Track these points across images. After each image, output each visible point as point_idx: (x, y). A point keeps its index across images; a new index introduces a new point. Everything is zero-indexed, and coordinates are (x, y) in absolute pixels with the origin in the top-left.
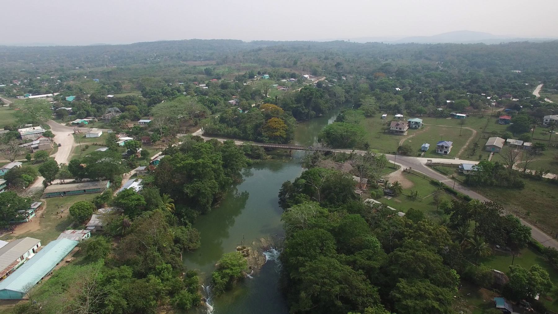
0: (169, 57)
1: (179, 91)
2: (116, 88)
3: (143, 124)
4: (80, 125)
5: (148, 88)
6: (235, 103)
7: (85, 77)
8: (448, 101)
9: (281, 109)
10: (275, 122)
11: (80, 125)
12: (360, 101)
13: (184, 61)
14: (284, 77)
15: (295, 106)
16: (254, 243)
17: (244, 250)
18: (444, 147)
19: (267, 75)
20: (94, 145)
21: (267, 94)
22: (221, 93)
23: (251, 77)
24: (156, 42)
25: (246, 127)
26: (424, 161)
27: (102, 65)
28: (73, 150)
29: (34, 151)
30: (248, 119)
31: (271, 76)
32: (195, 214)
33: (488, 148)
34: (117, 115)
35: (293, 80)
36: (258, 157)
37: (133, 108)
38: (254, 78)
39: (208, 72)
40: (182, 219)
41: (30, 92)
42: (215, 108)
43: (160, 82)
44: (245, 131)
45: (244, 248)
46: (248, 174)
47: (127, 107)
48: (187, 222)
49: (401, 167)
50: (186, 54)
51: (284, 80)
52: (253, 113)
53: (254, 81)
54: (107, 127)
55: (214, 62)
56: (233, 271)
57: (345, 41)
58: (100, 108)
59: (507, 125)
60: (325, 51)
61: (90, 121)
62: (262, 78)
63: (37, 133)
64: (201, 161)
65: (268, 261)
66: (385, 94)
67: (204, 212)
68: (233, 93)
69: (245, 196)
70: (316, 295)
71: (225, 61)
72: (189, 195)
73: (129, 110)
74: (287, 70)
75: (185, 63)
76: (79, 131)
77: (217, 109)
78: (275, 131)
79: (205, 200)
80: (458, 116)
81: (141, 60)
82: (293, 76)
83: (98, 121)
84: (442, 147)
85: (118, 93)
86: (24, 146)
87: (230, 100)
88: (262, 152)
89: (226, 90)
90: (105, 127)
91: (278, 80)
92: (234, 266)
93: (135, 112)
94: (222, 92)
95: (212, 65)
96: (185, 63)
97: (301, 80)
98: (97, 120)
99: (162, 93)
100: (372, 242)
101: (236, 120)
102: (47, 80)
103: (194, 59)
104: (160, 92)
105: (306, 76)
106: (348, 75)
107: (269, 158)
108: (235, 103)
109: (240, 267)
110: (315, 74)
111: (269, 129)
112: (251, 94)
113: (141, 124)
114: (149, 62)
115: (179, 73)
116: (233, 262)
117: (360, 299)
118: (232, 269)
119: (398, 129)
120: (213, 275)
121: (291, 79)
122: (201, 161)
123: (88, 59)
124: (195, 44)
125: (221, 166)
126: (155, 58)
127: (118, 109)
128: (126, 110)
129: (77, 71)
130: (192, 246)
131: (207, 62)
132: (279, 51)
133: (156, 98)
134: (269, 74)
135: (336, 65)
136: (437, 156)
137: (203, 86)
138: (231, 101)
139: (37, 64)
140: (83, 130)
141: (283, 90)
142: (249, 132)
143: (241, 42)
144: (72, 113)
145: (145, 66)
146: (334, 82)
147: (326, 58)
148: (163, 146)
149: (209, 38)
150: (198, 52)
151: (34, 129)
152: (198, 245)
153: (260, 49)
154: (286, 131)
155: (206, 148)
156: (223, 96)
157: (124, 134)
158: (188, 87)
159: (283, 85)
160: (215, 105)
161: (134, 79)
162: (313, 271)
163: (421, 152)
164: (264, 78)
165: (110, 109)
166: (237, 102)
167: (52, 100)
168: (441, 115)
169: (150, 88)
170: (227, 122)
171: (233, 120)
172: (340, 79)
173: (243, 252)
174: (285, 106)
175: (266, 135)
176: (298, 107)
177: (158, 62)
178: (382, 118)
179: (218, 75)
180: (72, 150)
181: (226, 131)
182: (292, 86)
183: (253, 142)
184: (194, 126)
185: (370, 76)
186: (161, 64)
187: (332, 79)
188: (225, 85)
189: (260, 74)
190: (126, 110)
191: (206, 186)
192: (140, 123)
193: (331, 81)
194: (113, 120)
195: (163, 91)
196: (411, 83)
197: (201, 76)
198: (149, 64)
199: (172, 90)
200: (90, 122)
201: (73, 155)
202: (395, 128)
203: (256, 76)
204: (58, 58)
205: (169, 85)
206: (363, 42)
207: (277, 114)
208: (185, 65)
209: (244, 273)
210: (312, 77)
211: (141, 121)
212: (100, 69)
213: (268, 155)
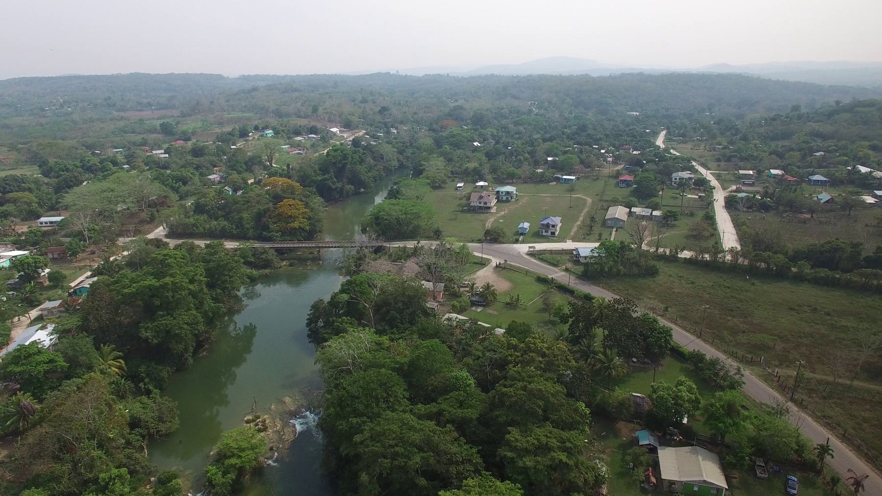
0: (89, 105)
1: (115, 163)
3: (49, 225)
6: (218, 179)
8: (549, 159)
9: (298, 184)
10: (290, 205)
12: (421, 165)
13: (119, 111)
14: (298, 133)
15: (319, 178)
16: (273, 406)
17: (258, 420)
18: (551, 226)
19: (271, 131)
21: (272, 161)
22: (193, 163)
23: (244, 134)
25: (241, 218)
26: (523, 248)
30: (244, 204)
31: (277, 132)
32: (165, 372)
33: (608, 222)
35: (314, 138)
36: (267, 264)
37: (22, 198)
39: (166, 130)
40: (142, 385)
42: (184, 189)
43: (76, 149)
44: (239, 224)
45: (258, 417)
46: (252, 296)
48: (151, 388)
49: (491, 260)
50: (122, 100)
51: (299, 138)
52: (251, 194)
53: (250, 141)
56: (243, 459)
57: (391, 73)
59: (630, 189)
65: (301, 433)
66: (459, 152)
67: (180, 366)
69: (251, 330)
70: (385, 475)
71: (195, 109)
72: (150, 341)
74: (303, 122)
75: (122, 114)
78: (290, 221)
79: (181, 347)
80: (565, 179)
82: (313, 130)
84: (548, 225)
87: (210, 175)
88: (272, 256)
89: (202, 159)
92: (243, 450)
94: (195, 162)
96: (122, 114)
97: (326, 138)
99: (82, 167)
100: (462, 379)
101: (222, 208)
103: (139, 108)
105: (334, 130)
106: (400, 126)
107: (285, 265)
108: (218, 179)
109: (253, 450)
110: (347, 125)
111: (282, 217)
112: (246, 163)
113: (44, 225)
115: (112, 133)
116: (241, 443)
117: (453, 470)
118: (240, 457)
119: (482, 203)
120: (207, 472)
124: (138, 82)
125: (204, 287)
130: (163, 428)
131: (163, 112)
134: (274, 129)
135: (380, 112)
136: (542, 240)
141: (299, 153)
142: (248, 226)
143: (220, 77)
145: (43, 121)
147: (364, 101)
152: (176, 423)
153: (255, 89)
154: (309, 219)
155: (175, 258)
156: (197, 168)
159: (298, 145)
162: (375, 438)
163: (519, 236)
164: (265, 135)
166: (222, 177)
168: (541, 180)
172: (388, 133)
173: (257, 425)
174: (304, 180)
176: (326, 179)
178: (457, 189)
179: (184, 133)
181: (208, 226)
182: (313, 146)
183: (256, 242)
185: (435, 126)
186: (75, 117)
187: (375, 133)
188: (199, 150)
189: (259, 129)
191: (181, 323)
192: (41, 223)
196: (496, 134)
197: (154, 136)
198: (49, 117)
202: (478, 203)
203: (251, 134)
206: (420, 74)
207: (292, 193)
209: (261, 459)
210: (343, 131)
211: (43, 219)
213: (283, 260)
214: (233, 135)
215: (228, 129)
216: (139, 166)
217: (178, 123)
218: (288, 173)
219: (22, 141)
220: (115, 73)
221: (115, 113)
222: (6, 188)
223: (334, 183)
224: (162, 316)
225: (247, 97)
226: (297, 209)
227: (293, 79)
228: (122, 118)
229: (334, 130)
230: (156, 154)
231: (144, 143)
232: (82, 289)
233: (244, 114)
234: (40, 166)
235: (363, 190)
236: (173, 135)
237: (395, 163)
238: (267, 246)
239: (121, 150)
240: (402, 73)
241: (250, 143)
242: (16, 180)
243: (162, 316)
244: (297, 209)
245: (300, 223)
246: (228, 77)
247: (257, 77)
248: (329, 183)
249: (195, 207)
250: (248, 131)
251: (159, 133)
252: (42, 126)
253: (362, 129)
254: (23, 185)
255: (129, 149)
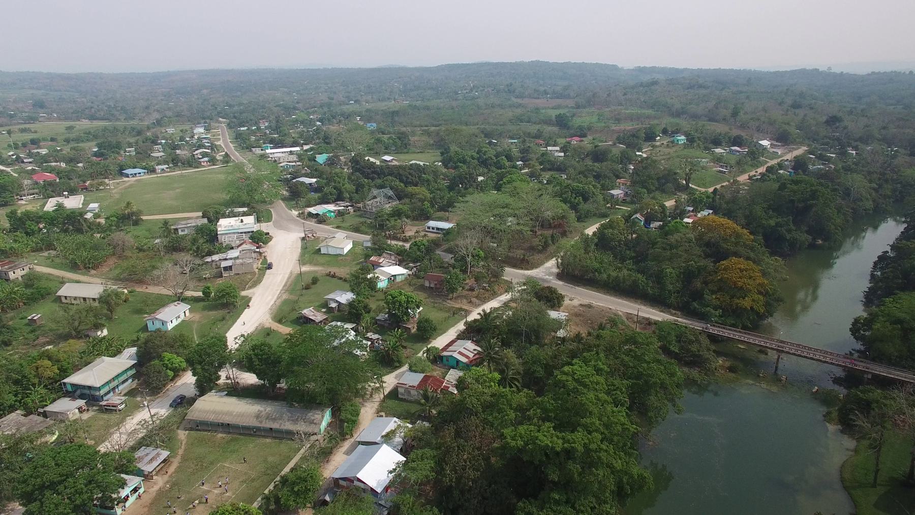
0: (493, 90)
1: (509, 158)
2: (399, 143)
3: (435, 231)
4: (320, 219)
5: (454, 148)
6: (622, 195)
7: (358, 118)
10: (742, 271)
11: (320, 219)
13: (517, 97)
14: (717, 143)
15: (772, 222)
19: (683, 137)
20: (329, 275)
22: (593, 170)
23: (650, 137)
24: (474, 64)
27: (389, 99)
28: (289, 283)
29: (225, 274)
31: (691, 140)
34: (388, 207)
35: (739, 152)
37: (419, 194)
38: (655, 140)
39: (562, 122)
41: (272, 141)
42: (584, 207)
43: (476, 136)
44: (659, 278)
47: (410, 189)
50: (522, 86)
53: (657, 146)
54: (366, 230)
55: (571, 103)
57: (820, 70)
58: (362, 186)
60: (787, 89)
61: (339, 210)
62: (673, 142)
63: (241, 233)
64: (578, 438)
68: (617, 173)
71: (591, 101)
73: (411, 196)
74: (720, 128)
75: (519, 101)
76: (314, 235)
77: (588, 211)
81: (448, 94)
82: (737, 141)
83: (354, 211)
85: (401, 153)
86: (213, 261)
87: (613, 189)
88: (705, 348)
90: (363, 228)
91: (706, 148)
93: (422, 201)
95: (567, 107)
96: (519, 101)
97: (756, 154)
98: (352, 211)
99: (478, 159)
102: (302, 123)
103: (536, 95)
104: (473, 159)
105: (765, 143)
106: (861, 146)
107: (722, 367)
110: (783, 139)
111: (723, 287)
113: (431, 230)
114: (461, 97)
115: (510, 120)
121: (733, 148)
122: (578, 438)
123: (369, 88)
124: (538, 70)
126: (471, 90)
127: (391, 193)
128: (406, 196)
129: (351, 107)
131: (559, 101)
132: (691, 87)
133: (466, 174)
134: (687, 135)
137: (555, 152)
138: (612, 192)
139: (301, 94)
140: (322, 230)
142: (670, 287)
143: (614, 67)
144: (316, 188)
145: (454, 104)
146: (829, 160)
147: (796, 106)
148: (471, 302)
149: (561, 60)
150: (541, 82)
151: (242, 221)
153: (655, 83)
154: (766, 294)
156: (597, 177)
157: (393, 258)
158: (527, 150)
159: (718, 160)
160: (586, 199)
161: (433, 126)
164: (676, 142)
165: (375, 192)
166: (626, 194)
167: (295, 159)
169: (457, 149)
170: (612, 249)
171: (626, 245)
172: (843, 153)
175: (716, 302)
177: (473, 98)
179: (581, 128)
180: (285, 285)
181: (614, 274)
182: (739, 163)
184: (540, 252)
186: (481, 102)
187: (824, 153)
190: (406, 196)
192: (429, 228)
193: (821, 158)
194: (378, 215)
195: (480, 157)
197: (550, 128)
198: (460, 100)
199: (497, 156)
200: (340, 214)
201: (285, 297)
203: (659, 138)
204: (330, 85)
205: (490, 143)
208: (520, 105)
211: (432, 223)
212: (383, 106)
214: (637, 137)
215: (628, 126)
216: (534, 166)
217: (574, 115)
218: (714, 200)
219: (435, 123)
220: (518, 60)
221: (514, 100)
222: (408, 178)
223: (789, 231)
224: (557, 502)
225: (646, 92)
226: (751, 278)
227: (700, 73)
228: (520, 105)
229: (765, 143)
230: (551, 151)
231: (538, 136)
232: (450, 358)
233: (644, 111)
234: (442, 154)
235: (820, 242)
236: (568, 128)
237: (869, 205)
238: (698, 326)
239: (516, 141)
240: (836, 70)
241: (658, 149)
242: (419, 170)
243: (557, 502)
244: (751, 278)
245: (753, 300)
246: (622, 69)
247: (653, 70)
248: (783, 230)
249: (598, 238)
250: (655, 134)
251: (553, 125)
252: (452, 109)
253: (802, 144)
254: (423, 175)
255: (524, 141)
